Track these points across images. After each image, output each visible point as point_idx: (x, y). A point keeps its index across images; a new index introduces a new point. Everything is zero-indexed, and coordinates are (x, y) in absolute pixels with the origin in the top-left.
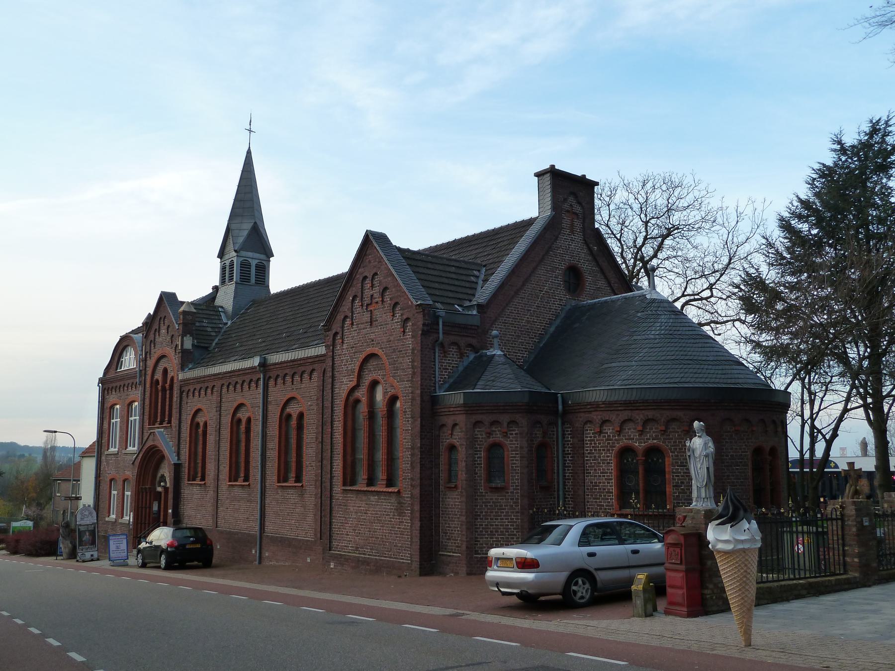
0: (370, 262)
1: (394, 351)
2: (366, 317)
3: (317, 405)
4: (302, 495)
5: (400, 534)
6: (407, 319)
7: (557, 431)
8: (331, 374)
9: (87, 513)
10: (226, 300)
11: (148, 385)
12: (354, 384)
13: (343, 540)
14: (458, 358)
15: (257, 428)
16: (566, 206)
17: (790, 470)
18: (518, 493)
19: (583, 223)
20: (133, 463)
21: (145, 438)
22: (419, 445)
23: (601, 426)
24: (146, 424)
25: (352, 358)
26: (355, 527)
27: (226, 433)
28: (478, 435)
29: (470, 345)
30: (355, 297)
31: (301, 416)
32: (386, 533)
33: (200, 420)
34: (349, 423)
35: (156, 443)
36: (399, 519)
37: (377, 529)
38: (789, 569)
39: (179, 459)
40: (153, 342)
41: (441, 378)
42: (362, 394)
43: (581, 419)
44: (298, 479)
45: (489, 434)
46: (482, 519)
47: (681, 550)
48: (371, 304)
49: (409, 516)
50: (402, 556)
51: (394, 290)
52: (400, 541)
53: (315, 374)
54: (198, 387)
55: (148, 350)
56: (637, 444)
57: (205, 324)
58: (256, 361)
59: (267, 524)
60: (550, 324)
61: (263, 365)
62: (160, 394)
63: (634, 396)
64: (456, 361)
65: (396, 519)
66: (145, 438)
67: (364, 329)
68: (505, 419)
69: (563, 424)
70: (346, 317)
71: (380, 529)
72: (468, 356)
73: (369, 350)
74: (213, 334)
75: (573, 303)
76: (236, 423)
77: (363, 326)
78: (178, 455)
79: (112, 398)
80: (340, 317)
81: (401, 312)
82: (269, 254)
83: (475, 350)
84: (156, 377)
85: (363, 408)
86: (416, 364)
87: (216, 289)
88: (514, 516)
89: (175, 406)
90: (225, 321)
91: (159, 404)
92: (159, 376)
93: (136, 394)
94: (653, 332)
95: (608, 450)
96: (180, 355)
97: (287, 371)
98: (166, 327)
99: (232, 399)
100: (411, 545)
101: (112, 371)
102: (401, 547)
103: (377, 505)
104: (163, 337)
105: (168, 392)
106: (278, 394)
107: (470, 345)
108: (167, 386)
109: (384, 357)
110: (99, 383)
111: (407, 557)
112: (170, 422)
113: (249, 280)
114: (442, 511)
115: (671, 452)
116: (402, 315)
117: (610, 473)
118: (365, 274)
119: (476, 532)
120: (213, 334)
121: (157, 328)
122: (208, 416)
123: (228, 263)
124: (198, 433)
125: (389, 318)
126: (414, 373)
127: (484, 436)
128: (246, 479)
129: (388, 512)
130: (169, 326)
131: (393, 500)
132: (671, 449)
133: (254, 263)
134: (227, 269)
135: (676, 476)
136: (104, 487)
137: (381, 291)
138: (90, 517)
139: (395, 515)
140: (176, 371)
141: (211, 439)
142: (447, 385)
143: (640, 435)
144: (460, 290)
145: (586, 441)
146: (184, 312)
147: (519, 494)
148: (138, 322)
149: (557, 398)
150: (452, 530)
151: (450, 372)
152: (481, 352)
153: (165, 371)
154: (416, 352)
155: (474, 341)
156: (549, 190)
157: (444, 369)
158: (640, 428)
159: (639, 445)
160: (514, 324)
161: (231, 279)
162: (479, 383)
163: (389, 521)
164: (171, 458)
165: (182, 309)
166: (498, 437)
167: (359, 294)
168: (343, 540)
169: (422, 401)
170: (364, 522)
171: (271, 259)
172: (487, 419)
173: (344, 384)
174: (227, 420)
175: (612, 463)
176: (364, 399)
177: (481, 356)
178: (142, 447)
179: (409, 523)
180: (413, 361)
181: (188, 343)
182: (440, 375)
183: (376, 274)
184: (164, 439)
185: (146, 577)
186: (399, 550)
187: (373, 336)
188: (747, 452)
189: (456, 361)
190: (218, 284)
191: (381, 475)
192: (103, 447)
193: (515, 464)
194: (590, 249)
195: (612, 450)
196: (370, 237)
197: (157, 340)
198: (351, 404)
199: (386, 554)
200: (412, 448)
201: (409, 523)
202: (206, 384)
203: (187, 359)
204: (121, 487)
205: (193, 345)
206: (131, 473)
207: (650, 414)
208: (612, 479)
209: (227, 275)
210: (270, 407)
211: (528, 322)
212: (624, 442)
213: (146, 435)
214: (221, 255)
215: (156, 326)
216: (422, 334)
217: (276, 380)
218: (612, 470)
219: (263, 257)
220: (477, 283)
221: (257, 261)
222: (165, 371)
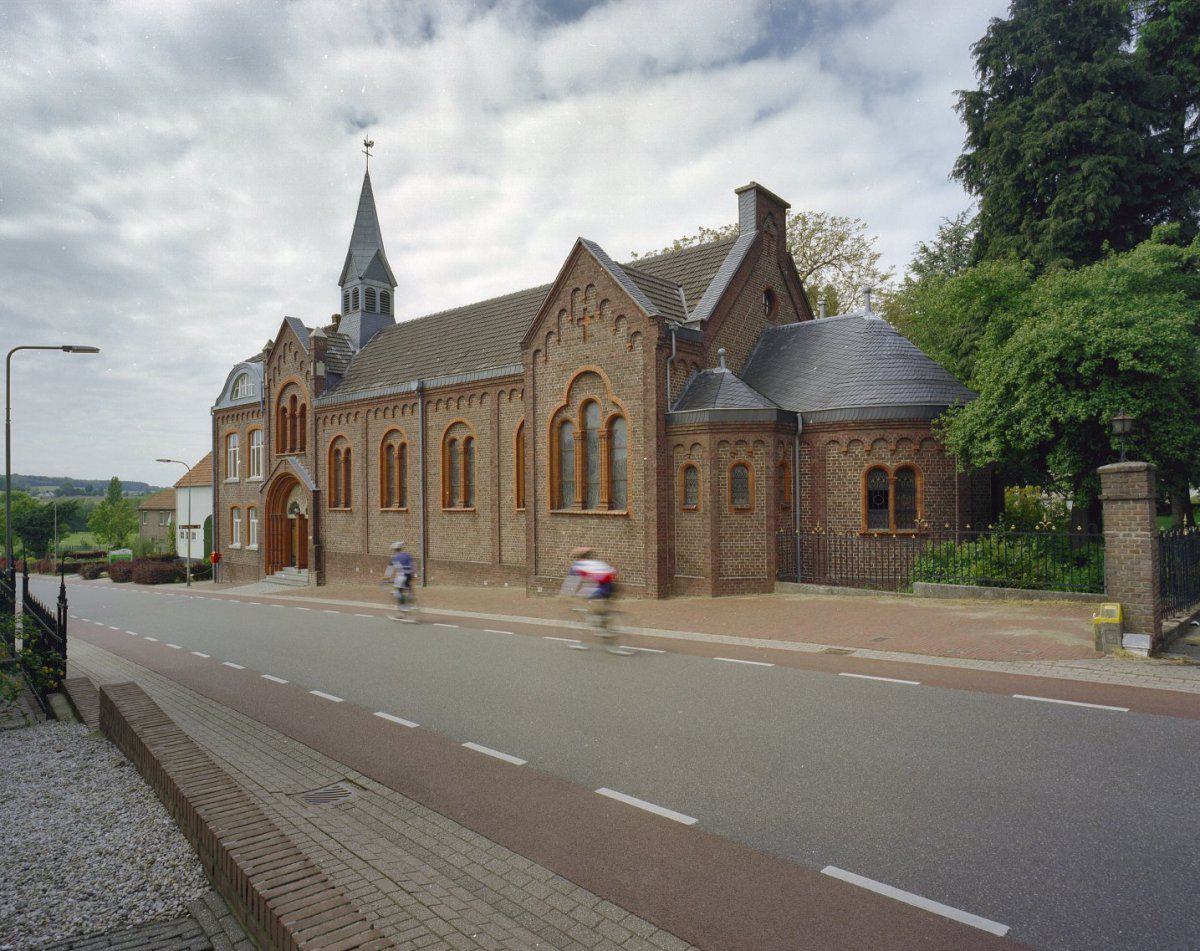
0: (582, 272)
1: (618, 367)
2: (578, 332)
3: (492, 428)
4: (474, 521)
6: (637, 333)
7: (794, 451)
8: (532, 394)
10: (352, 328)
11: (273, 412)
12: (564, 403)
15: (414, 455)
20: (261, 491)
21: (274, 467)
23: (849, 445)
24: (274, 449)
25: (559, 378)
27: (375, 460)
29: (695, 364)
30: (563, 311)
31: (348, 451)
34: (556, 444)
35: (288, 471)
39: (317, 486)
43: (823, 439)
45: (734, 454)
48: (583, 318)
53: (487, 399)
55: (271, 377)
56: (888, 464)
58: (414, 386)
59: (431, 548)
60: (754, 346)
61: (422, 390)
62: (289, 422)
66: (273, 469)
68: (751, 438)
69: (800, 443)
70: (550, 333)
77: (572, 343)
78: (316, 482)
79: (227, 428)
82: (393, 284)
83: (699, 368)
85: (572, 433)
87: (337, 318)
91: (289, 432)
92: (286, 403)
93: (260, 422)
96: (313, 381)
99: (380, 426)
105: (298, 420)
108: (298, 412)
109: (604, 375)
112: (303, 449)
113: (374, 309)
122: (352, 440)
123: (351, 291)
124: (340, 461)
125: (610, 331)
126: (647, 390)
127: (728, 456)
131: (620, 522)
133: (378, 292)
140: (308, 398)
142: (676, 404)
143: (892, 455)
146: (315, 337)
148: (258, 347)
149: (796, 418)
152: (703, 371)
153: (294, 399)
154: (649, 368)
155: (697, 359)
156: (753, 208)
158: (893, 447)
159: (891, 465)
161: (356, 307)
165: (313, 334)
166: (743, 457)
169: (658, 420)
171: (395, 288)
172: (733, 438)
173: (549, 407)
174: (375, 447)
176: (576, 420)
177: (706, 375)
180: (645, 378)
181: (321, 369)
183: (591, 285)
184: (298, 466)
187: (588, 353)
190: (339, 312)
192: (220, 476)
197: (277, 378)
198: (559, 423)
203: (321, 385)
205: (325, 372)
206: (259, 501)
207: (904, 433)
212: (873, 462)
214: (342, 282)
215: (280, 352)
216: (656, 349)
217: (437, 404)
219: (388, 286)
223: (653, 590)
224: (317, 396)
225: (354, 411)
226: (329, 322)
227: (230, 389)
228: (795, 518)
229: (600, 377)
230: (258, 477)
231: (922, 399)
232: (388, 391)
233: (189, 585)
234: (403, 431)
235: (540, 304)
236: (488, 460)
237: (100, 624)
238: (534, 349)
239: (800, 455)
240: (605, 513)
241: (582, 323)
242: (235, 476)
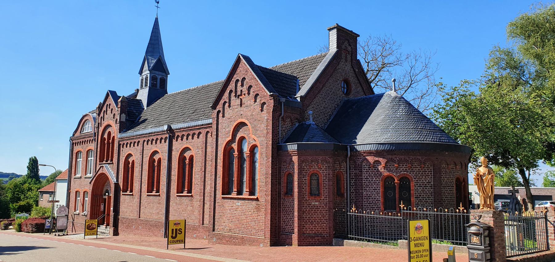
2: (238, 101)
3: (202, 151)
5: (258, 222)
9: (63, 209)
13: (222, 225)
14: (290, 125)
15: (164, 164)
17: (524, 188)
18: (327, 200)
19: (351, 57)
20: (90, 183)
21: (97, 170)
22: (270, 172)
24: (98, 160)
26: (229, 218)
28: (304, 167)
30: (231, 91)
32: (249, 221)
35: (103, 172)
36: (257, 214)
37: (243, 219)
38: (508, 246)
41: (282, 136)
42: (235, 146)
44: (190, 191)
46: (307, 214)
47: (481, 237)
49: (263, 212)
50: (259, 235)
51: (255, 87)
52: (258, 226)
54: (129, 142)
55: (100, 122)
57: (133, 109)
58: (165, 128)
63: (381, 148)
64: (289, 127)
65: (255, 213)
66: (97, 170)
67: (236, 108)
71: (245, 219)
72: (295, 124)
73: (240, 120)
74: (137, 114)
75: (346, 99)
76: (151, 161)
79: (77, 148)
80: (222, 102)
81: (260, 99)
82: (166, 72)
86: (269, 127)
88: (325, 212)
92: (106, 136)
94: (398, 114)
95: (378, 177)
96: (119, 124)
97: (184, 133)
98: (110, 109)
99: (149, 149)
100: (265, 228)
101: (78, 134)
102: (258, 229)
103: (243, 206)
105: (111, 144)
106: (178, 146)
110: (70, 140)
111: (262, 235)
114: (283, 209)
115: (414, 179)
116: (260, 101)
117: (379, 189)
118: (237, 78)
119: (303, 221)
120: (137, 114)
121: (105, 110)
122: (136, 158)
123: (144, 77)
124: (129, 168)
126: (268, 133)
128: (158, 191)
129: (250, 210)
130: (112, 109)
131: (254, 203)
132: (414, 177)
133: (159, 77)
135: (417, 192)
137: (247, 87)
138: (64, 212)
139: (255, 212)
145: (364, 171)
147: (327, 200)
150: (288, 220)
151: (286, 133)
153: (109, 133)
157: (283, 131)
160: (317, 108)
162: (304, 139)
163: (251, 215)
164: (113, 179)
167: (234, 90)
168: (222, 225)
170: (235, 215)
175: (380, 184)
178: (96, 174)
179: (263, 216)
182: (281, 134)
184: (110, 171)
186: (257, 231)
187: (242, 113)
188: (453, 179)
189: (289, 127)
193: (325, 183)
194: (354, 70)
195: (380, 177)
196: (241, 57)
198: (228, 151)
199: (248, 233)
200: (267, 174)
201: (263, 216)
202: (152, 138)
203: (124, 127)
206: (89, 188)
208: (380, 193)
209: (144, 83)
210: (173, 153)
215: (104, 109)
218: (380, 188)
219: (164, 74)
220: (296, 86)
221: (161, 76)
223: (268, 241)
224: (120, 132)
225: (197, 132)
228: (347, 203)
229: (247, 125)
231: (414, 139)
232: (154, 130)
233: (50, 234)
234: (159, 152)
235: (220, 88)
236: (199, 168)
238: (217, 110)
239: (350, 168)
240: (246, 197)
241: (240, 97)
242: (90, 174)
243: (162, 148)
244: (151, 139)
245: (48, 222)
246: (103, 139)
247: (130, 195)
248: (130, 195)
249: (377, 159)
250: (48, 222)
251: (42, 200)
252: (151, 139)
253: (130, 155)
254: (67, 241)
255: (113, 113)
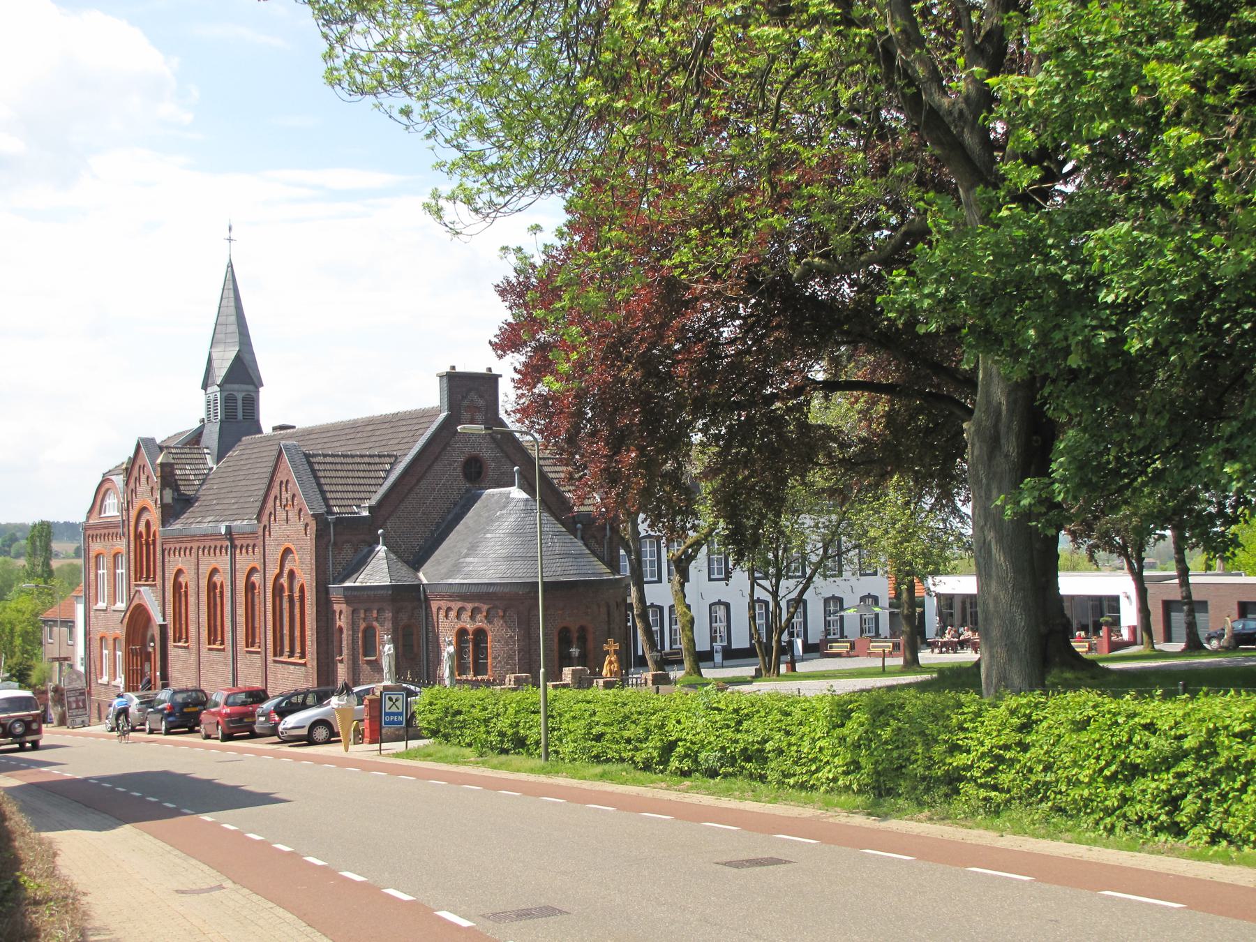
12: (277, 571)
15: (228, 594)
16: (466, 403)
20: (122, 622)
30: (276, 498)
33: (182, 579)
39: (164, 620)
40: (134, 491)
42: (284, 581)
55: (130, 499)
60: (449, 512)
82: (256, 383)
84: (140, 529)
89: (159, 564)
90: (210, 465)
92: (142, 528)
99: (208, 563)
104: (143, 488)
107: (364, 541)
123: (212, 397)
133: (240, 396)
134: (212, 403)
136: (95, 645)
141: (192, 600)
144: (362, 488)
159: (470, 627)
164: (158, 619)
171: (261, 389)
174: (204, 583)
176: (286, 585)
181: (168, 497)
184: (150, 598)
185: (287, 755)
191: (298, 650)
197: (134, 500)
203: (170, 513)
204: (112, 647)
205: (173, 498)
206: (121, 632)
211: (424, 514)
213: (133, 591)
214: (205, 386)
215: (135, 473)
219: (251, 387)
221: (244, 394)
222: (148, 524)
226: (198, 425)
227: (98, 507)
230: (121, 606)
237: (138, 794)
243: (223, 562)
244: (206, 542)
245: (390, 699)
246: (138, 536)
247: (185, 647)
248: (185, 647)
249: (476, 605)
250: (390, 699)
251: (50, 641)
252: (206, 542)
253: (179, 572)
254: (86, 735)
255: (150, 486)
